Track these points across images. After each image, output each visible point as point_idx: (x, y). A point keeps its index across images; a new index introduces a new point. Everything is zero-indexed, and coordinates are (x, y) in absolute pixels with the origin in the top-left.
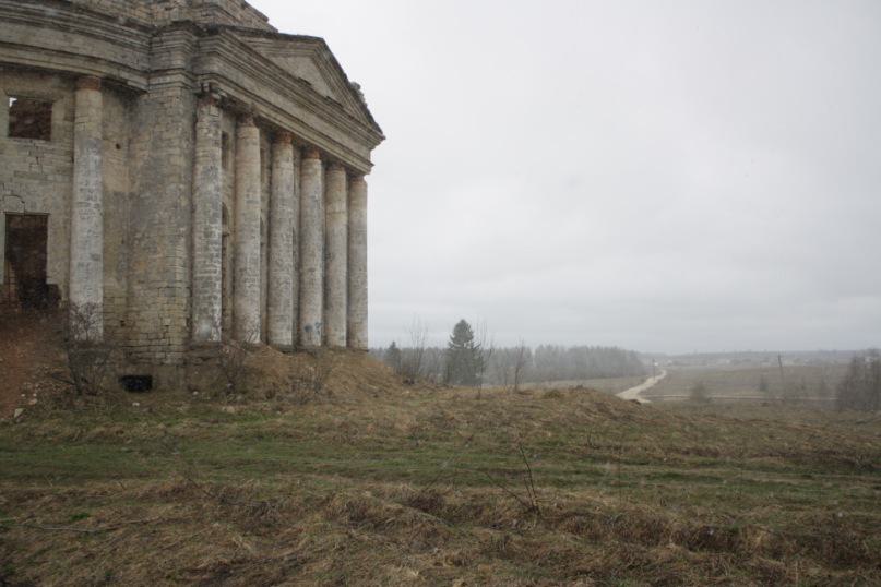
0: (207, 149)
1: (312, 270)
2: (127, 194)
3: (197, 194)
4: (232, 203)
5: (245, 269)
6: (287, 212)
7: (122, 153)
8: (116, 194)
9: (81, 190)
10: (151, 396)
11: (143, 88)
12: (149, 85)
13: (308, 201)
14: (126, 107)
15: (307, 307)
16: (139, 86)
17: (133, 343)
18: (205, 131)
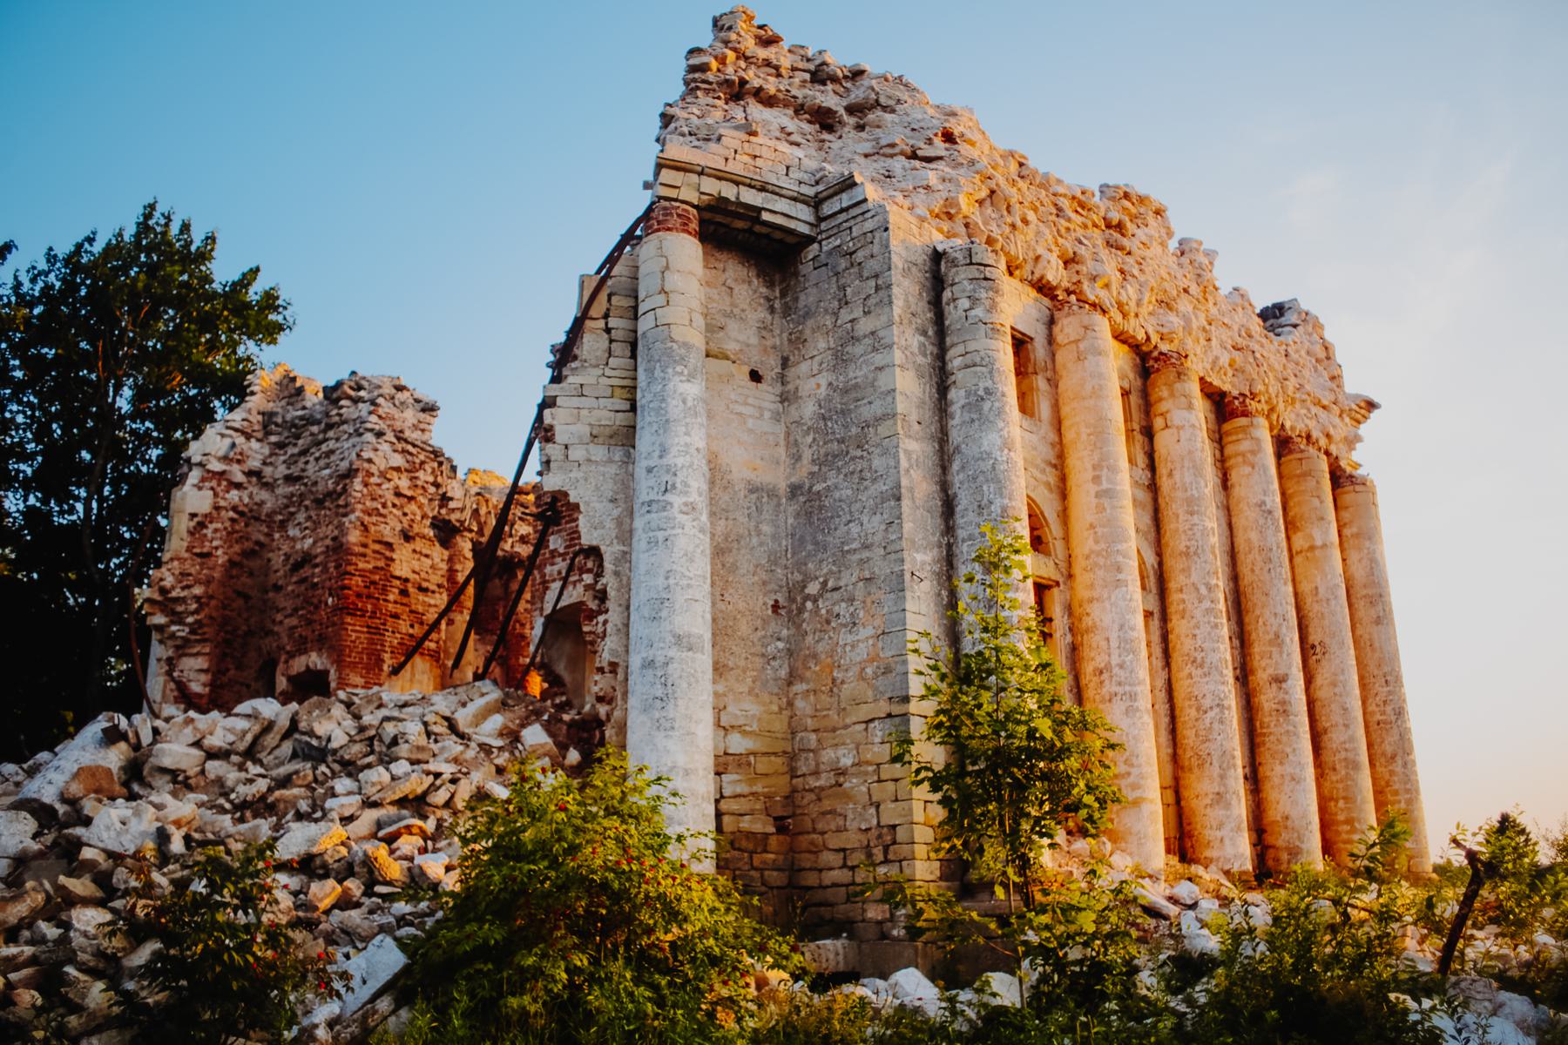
0: (972, 346)
1: (1280, 680)
2: (783, 486)
3: (956, 466)
4: (1057, 505)
5: (1108, 667)
6: (1200, 528)
7: (766, 394)
8: (754, 489)
9: (650, 470)
10: (1276, 780)
11: (804, 229)
12: (820, 219)
13: (1246, 517)
14: (770, 285)
15: (1273, 771)
16: (792, 225)
17: (811, 879)
18: (964, 303)
